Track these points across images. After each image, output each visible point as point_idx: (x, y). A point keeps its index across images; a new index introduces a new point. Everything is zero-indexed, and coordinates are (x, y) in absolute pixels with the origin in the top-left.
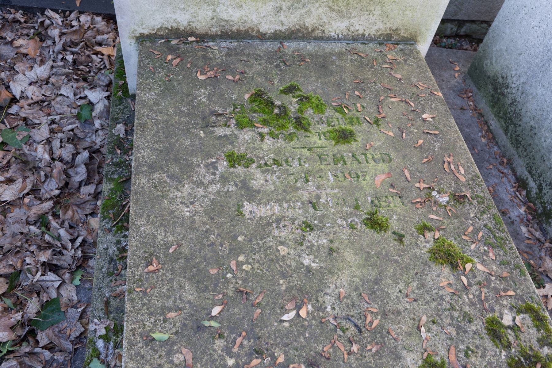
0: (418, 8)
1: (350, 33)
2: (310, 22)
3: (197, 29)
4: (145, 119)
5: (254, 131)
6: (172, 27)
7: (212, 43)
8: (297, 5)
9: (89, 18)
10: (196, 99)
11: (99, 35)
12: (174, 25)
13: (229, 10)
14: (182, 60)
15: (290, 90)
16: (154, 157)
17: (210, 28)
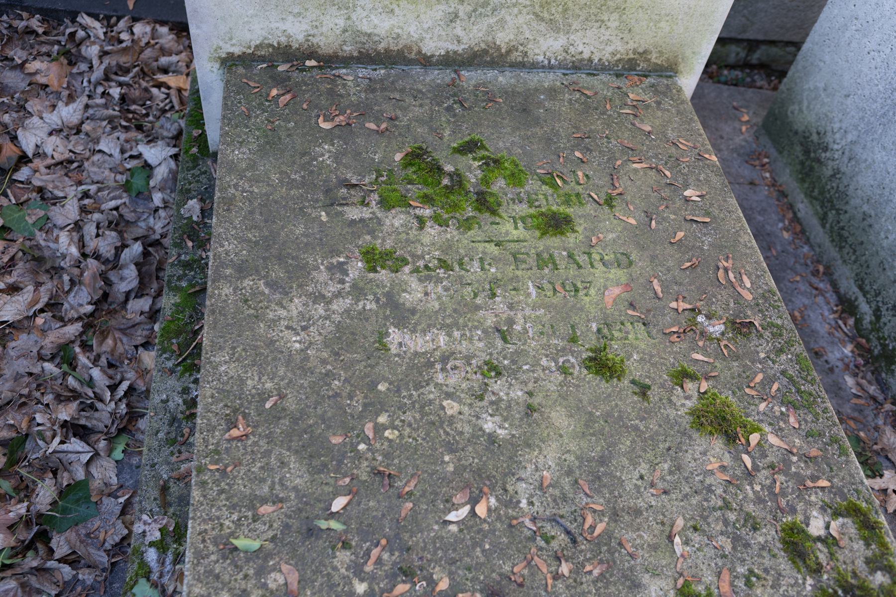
2: (503, 38)
3: (319, 47)
4: (232, 191)
5: (409, 213)
6: (279, 43)
7: (344, 71)
9: (148, 29)
10: (316, 160)
11: (164, 55)
12: (283, 39)
13: (373, 17)
14: (294, 97)
15: (470, 147)
16: (244, 252)
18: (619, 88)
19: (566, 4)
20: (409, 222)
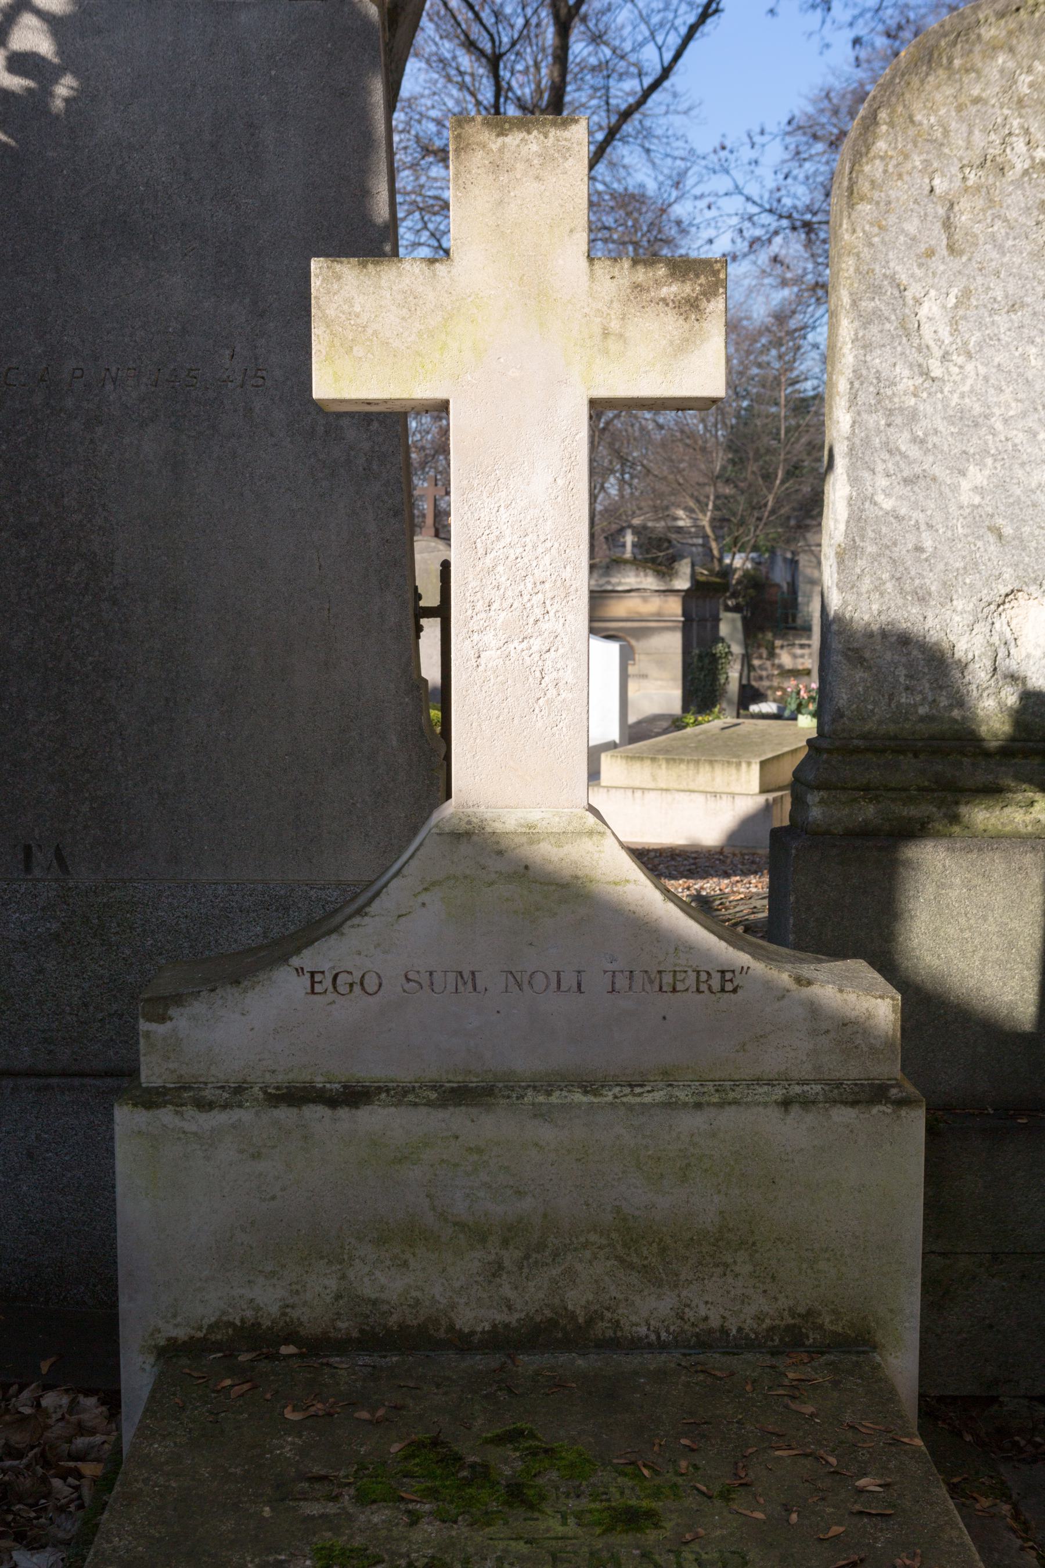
0: (846, 1252)
1: (686, 1327)
2: (577, 1299)
3: (301, 1324)
4: (140, 1485)
5: (398, 1508)
6: (242, 1321)
7: (338, 1359)
8: (539, 1257)
9: (65, 1400)
10: (271, 1452)
11: (82, 1435)
12: (249, 1314)
13: (378, 1273)
14: (254, 1387)
15: (513, 1437)
16: (140, 1549)
17: (334, 1320)
18: (772, 1367)
19: (661, 1240)
20: (396, 1517)
